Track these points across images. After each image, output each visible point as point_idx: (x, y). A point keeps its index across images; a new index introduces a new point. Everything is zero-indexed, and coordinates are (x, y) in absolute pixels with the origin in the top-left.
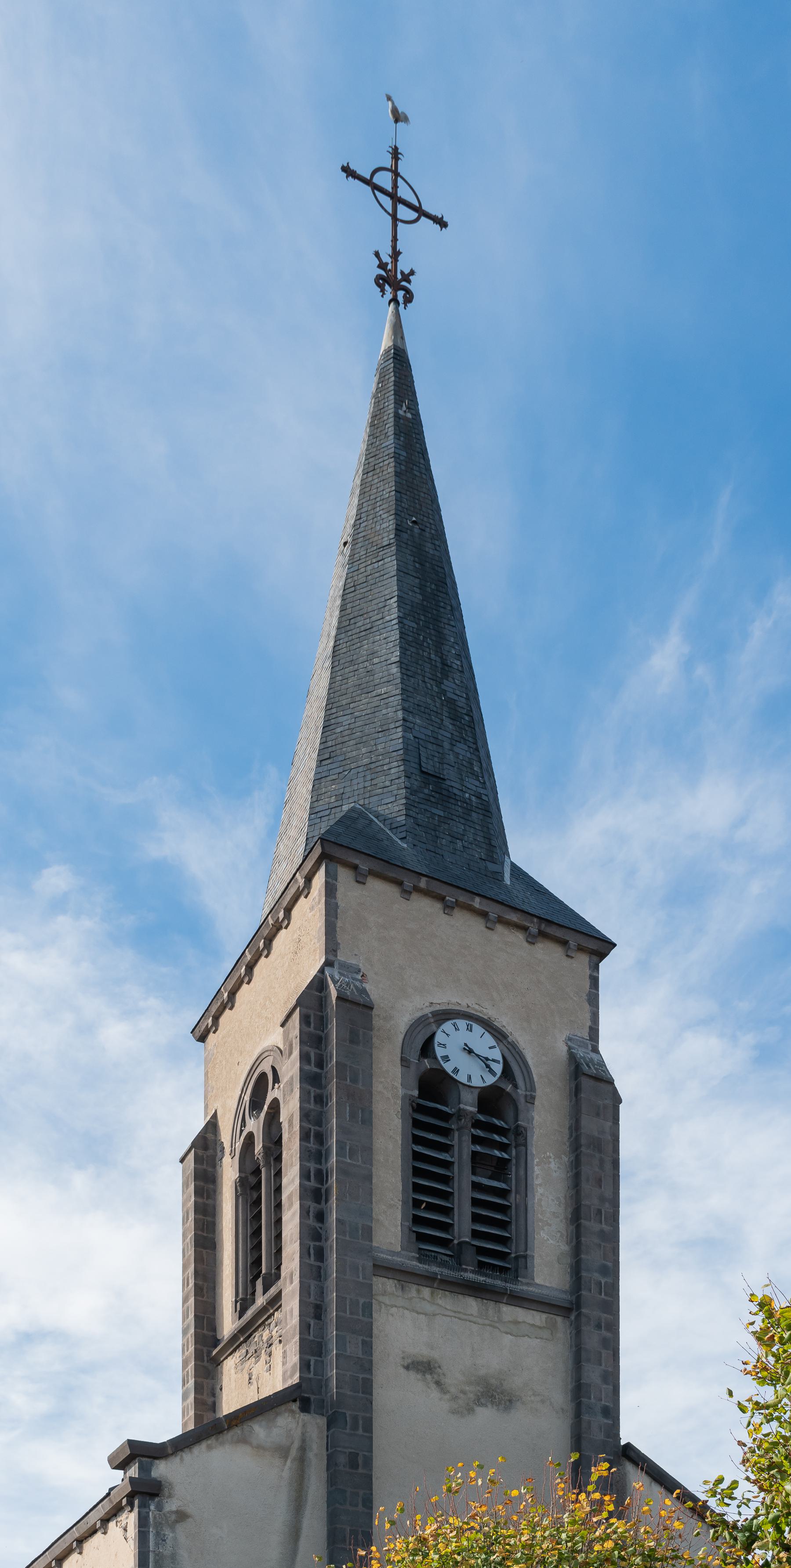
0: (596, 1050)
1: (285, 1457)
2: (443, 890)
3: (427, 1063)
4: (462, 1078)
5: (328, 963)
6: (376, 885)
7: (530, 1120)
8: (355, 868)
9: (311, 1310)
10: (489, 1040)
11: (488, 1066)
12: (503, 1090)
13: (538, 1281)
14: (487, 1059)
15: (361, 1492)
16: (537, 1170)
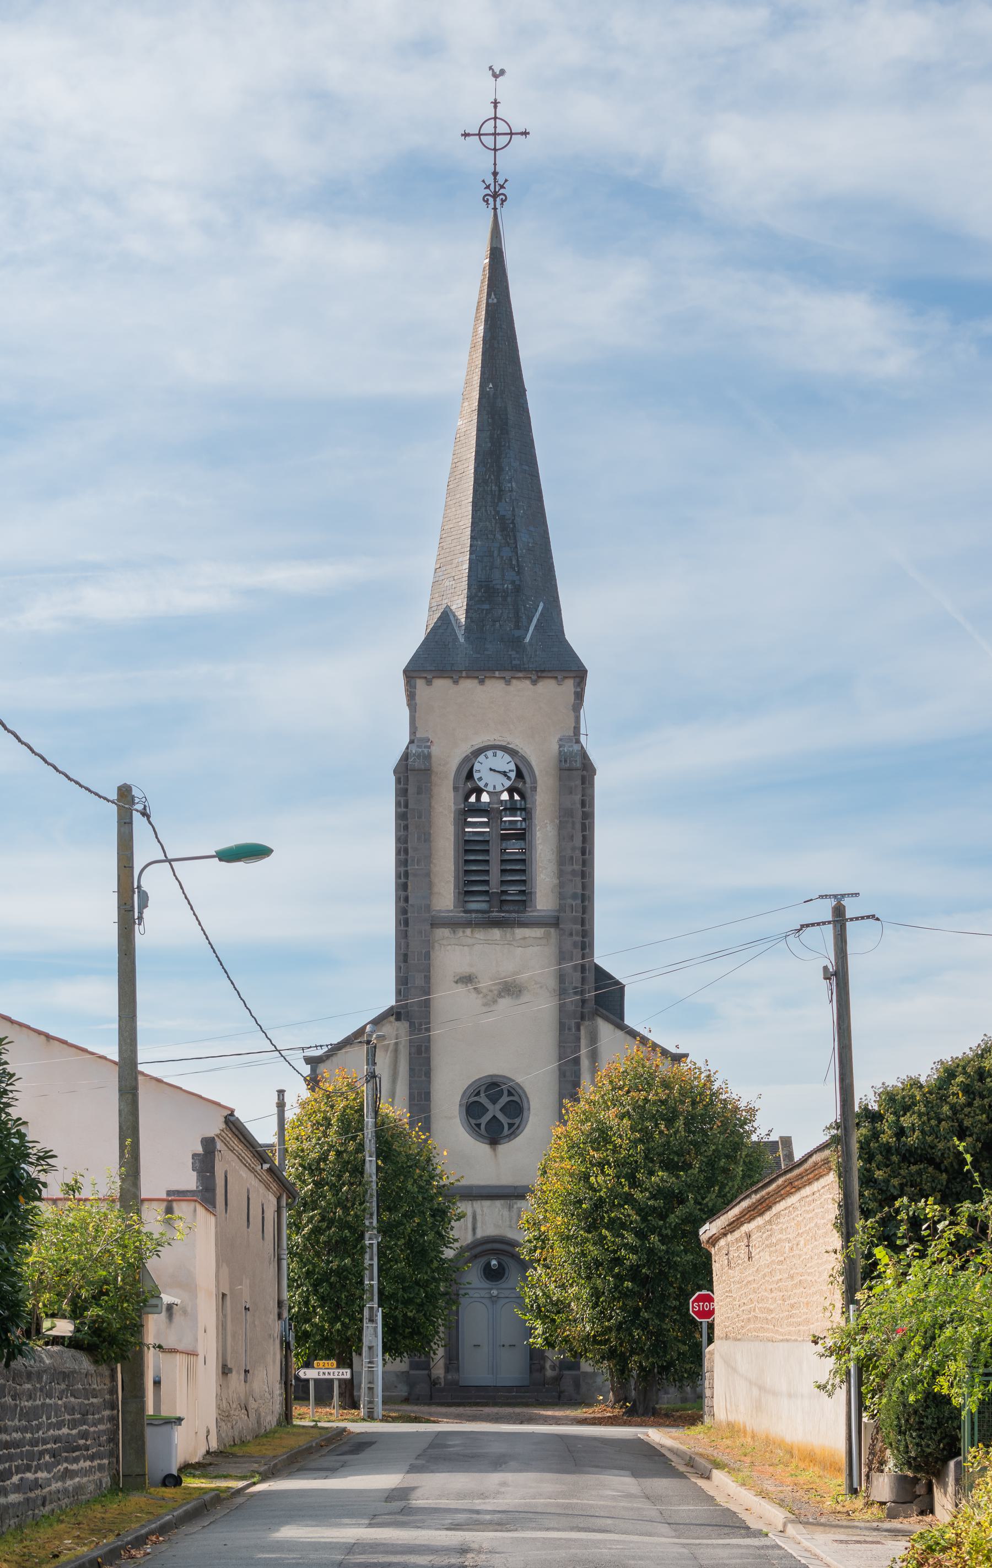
0: (578, 741)
2: (476, 674)
5: (411, 742)
7: (534, 802)
9: (402, 958)
10: (507, 758)
11: (506, 775)
13: (538, 908)
14: (505, 772)
16: (538, 834)
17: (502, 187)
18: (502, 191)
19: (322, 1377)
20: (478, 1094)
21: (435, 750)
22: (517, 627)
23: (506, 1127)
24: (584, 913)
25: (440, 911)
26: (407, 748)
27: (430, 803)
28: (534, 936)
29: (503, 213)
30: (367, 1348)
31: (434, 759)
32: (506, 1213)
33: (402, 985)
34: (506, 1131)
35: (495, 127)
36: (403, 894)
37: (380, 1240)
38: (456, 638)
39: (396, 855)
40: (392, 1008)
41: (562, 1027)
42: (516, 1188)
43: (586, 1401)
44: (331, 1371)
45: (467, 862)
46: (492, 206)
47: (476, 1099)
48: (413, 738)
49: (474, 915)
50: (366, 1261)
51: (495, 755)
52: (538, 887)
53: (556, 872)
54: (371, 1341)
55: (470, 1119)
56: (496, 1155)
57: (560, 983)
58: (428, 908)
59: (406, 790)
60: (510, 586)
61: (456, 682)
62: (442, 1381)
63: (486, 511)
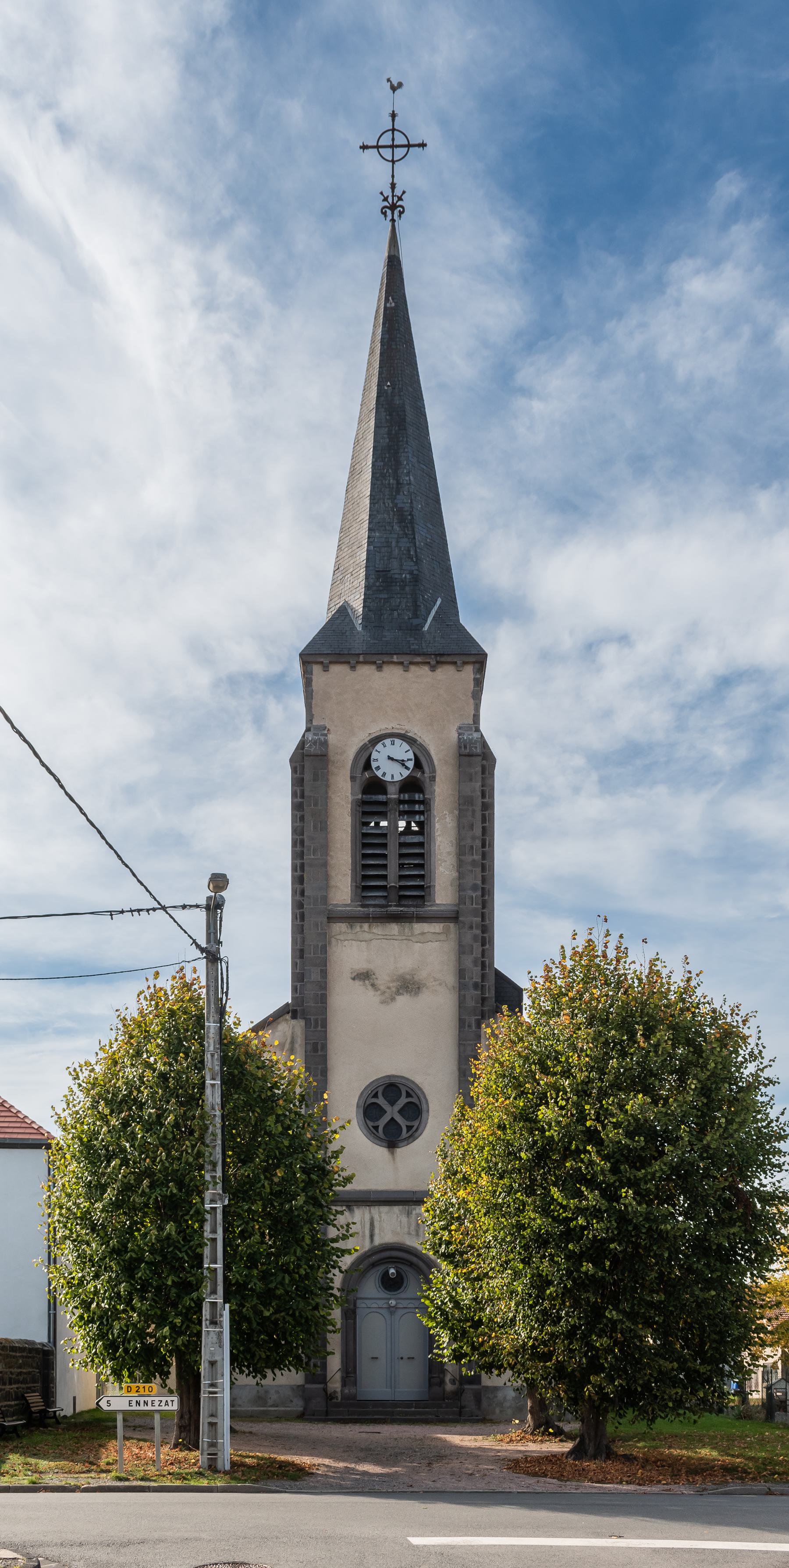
0: (478, 730)
1: (282, 1050)
2: (374, 658)
3: (367, 775)
4: (388, 778)
5: (308, 730)
6: (336, 669)
7: (433, 792)
8: (322, 663)
9: (298, 953)
10: (406, 746)
11: (403, 765)
12: (415, 777)
13: (438, 902)
14: (403, 761)
15: (320, 1067)
16: (437, 826)
17: (400, 199)
18: (400, 203)
19: (134, 1407)
20: (376, 1096)
21: (332, 738)
22: (416, 616)
23: (404, 1129)
24: (484, 907)
25: (336, 905)
26: (304, 736)
27: (327, 793)
28: (433, 931)
29: (400, 224)
30: (207, 1365)
31: (330, 747)
32: (404, 1219)
33: (299, 982)
34: (404, 1134)
35: (393, 139)
36: (299, 887)
37: (226, 1202)
38: (353, 627)
39: (293, 847)
40: (287, 1005)
41: (462, 1023)
42: (414, 1193)
43: (487, 1417)
44: (149, 1399)
45: (365, 856)
46: (389, 217)
47: (374, 1100)
48: (309, 725)
49: (371, 909)
50: (205, 1234)
51: (393, 743)
52: (437, 880)
53: (455, 864)
54: (212, 1354)
55: (368, 1121)
56: (394, 1159)
57: (460, 978)
58: (325, 899)
59: (303, 779)
60: (408, 576)
61: (353, 668)
62: (339, 1395)
63: (384, 503)
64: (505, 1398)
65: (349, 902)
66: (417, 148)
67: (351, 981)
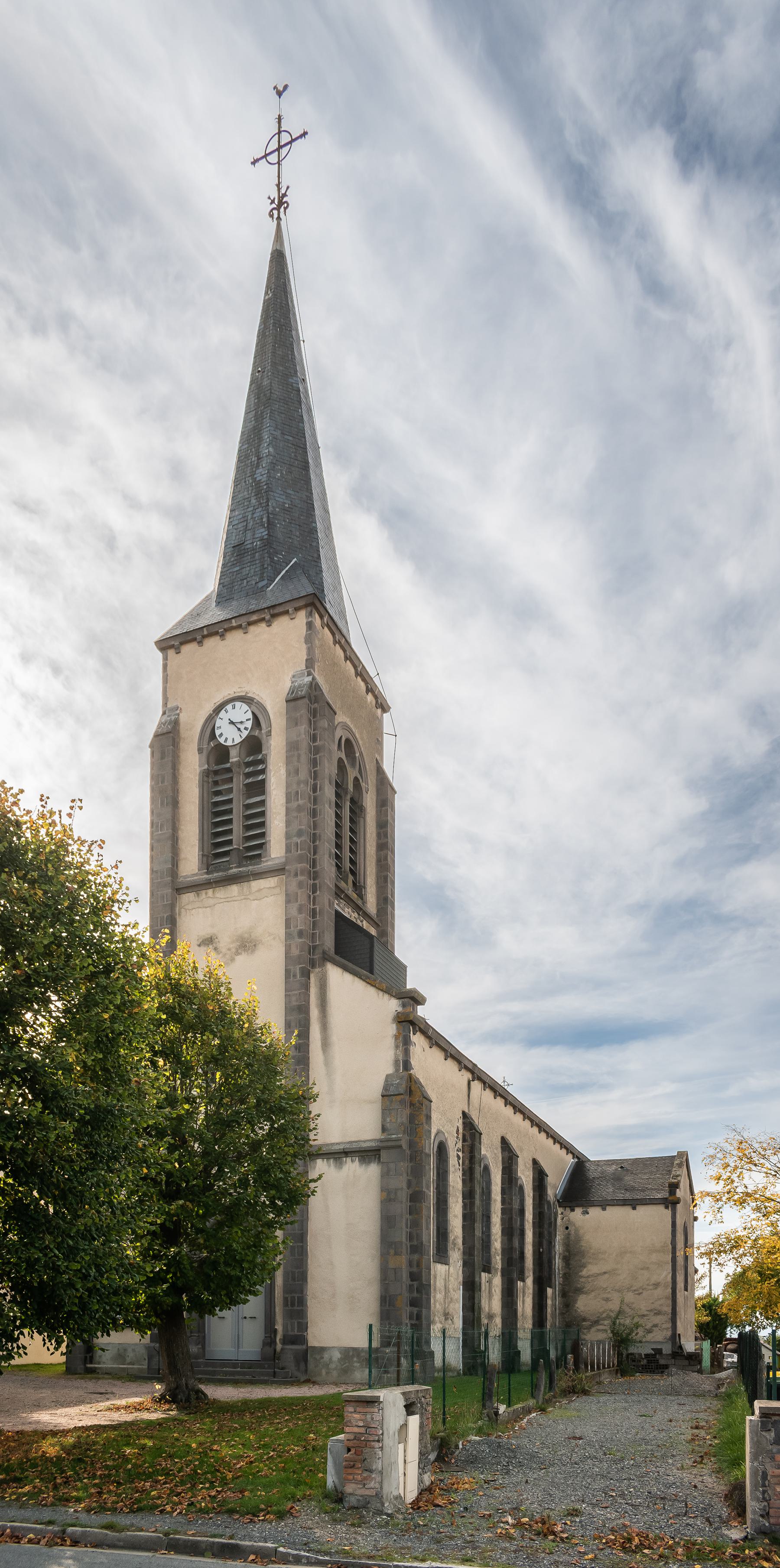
4: (229, 743)
5: (164, 713)
10: (245, 707)
12: (254, 736)
13: (273, 856)
21: (183, 718)
25: (186, 877)
52: (272, 835)
61: (200, 643)
64: (331, 1359)
65: (197, 871)
66: (300, 140)
67: (197, 948)
